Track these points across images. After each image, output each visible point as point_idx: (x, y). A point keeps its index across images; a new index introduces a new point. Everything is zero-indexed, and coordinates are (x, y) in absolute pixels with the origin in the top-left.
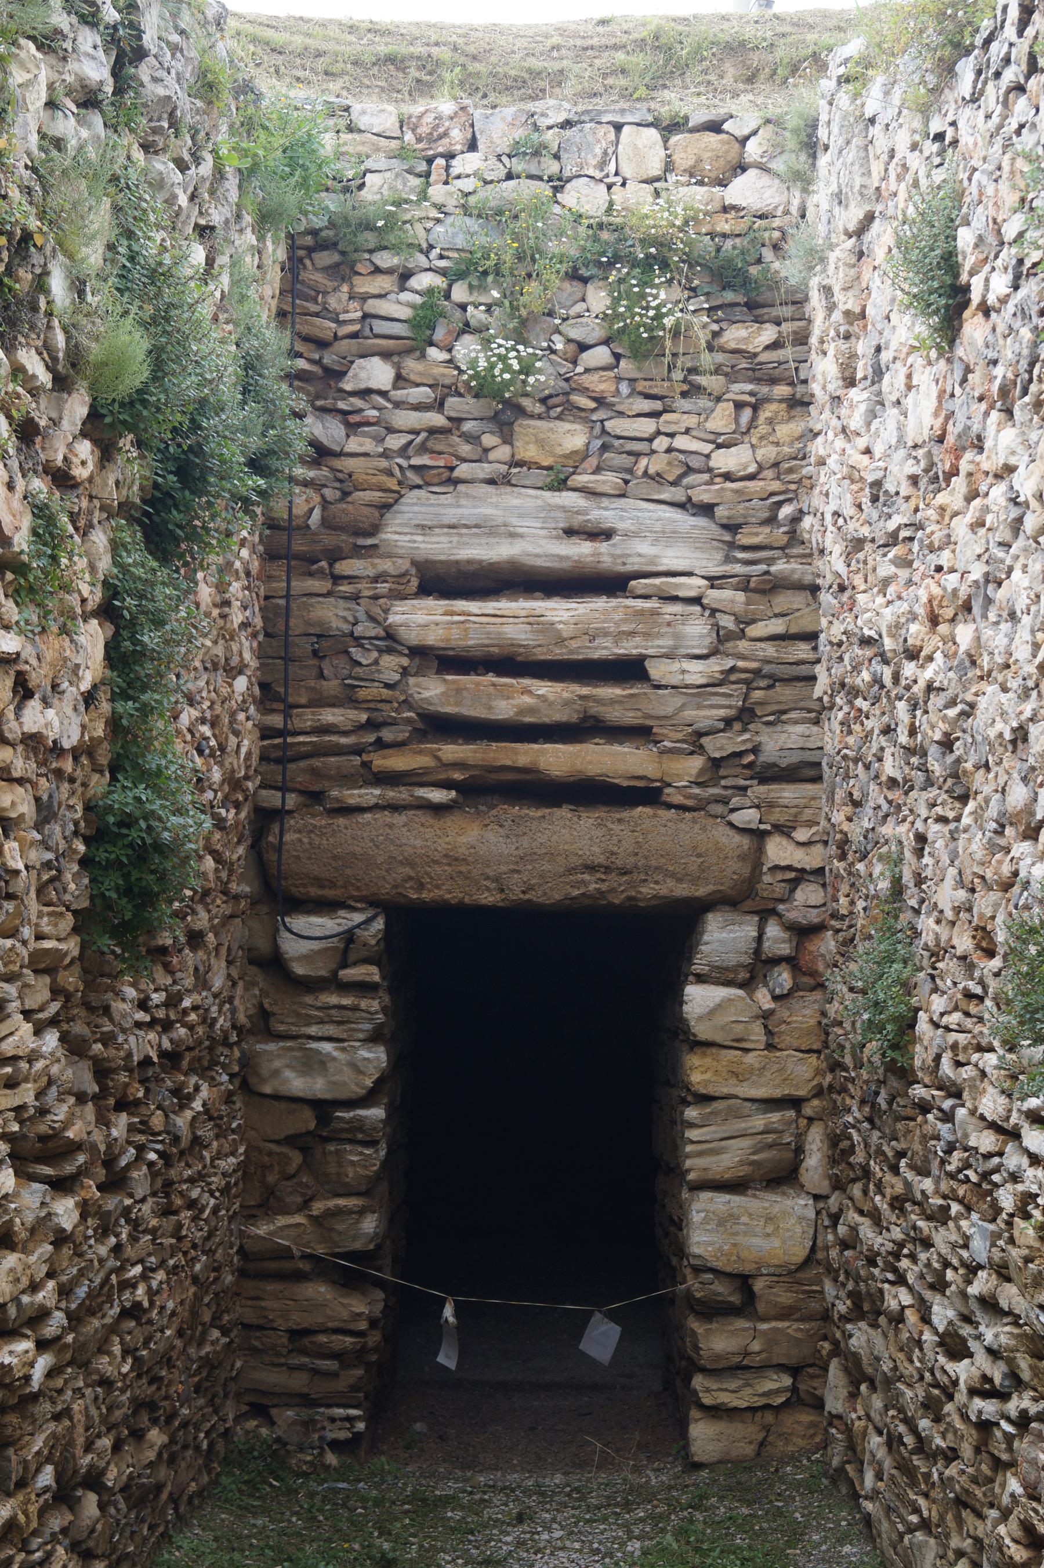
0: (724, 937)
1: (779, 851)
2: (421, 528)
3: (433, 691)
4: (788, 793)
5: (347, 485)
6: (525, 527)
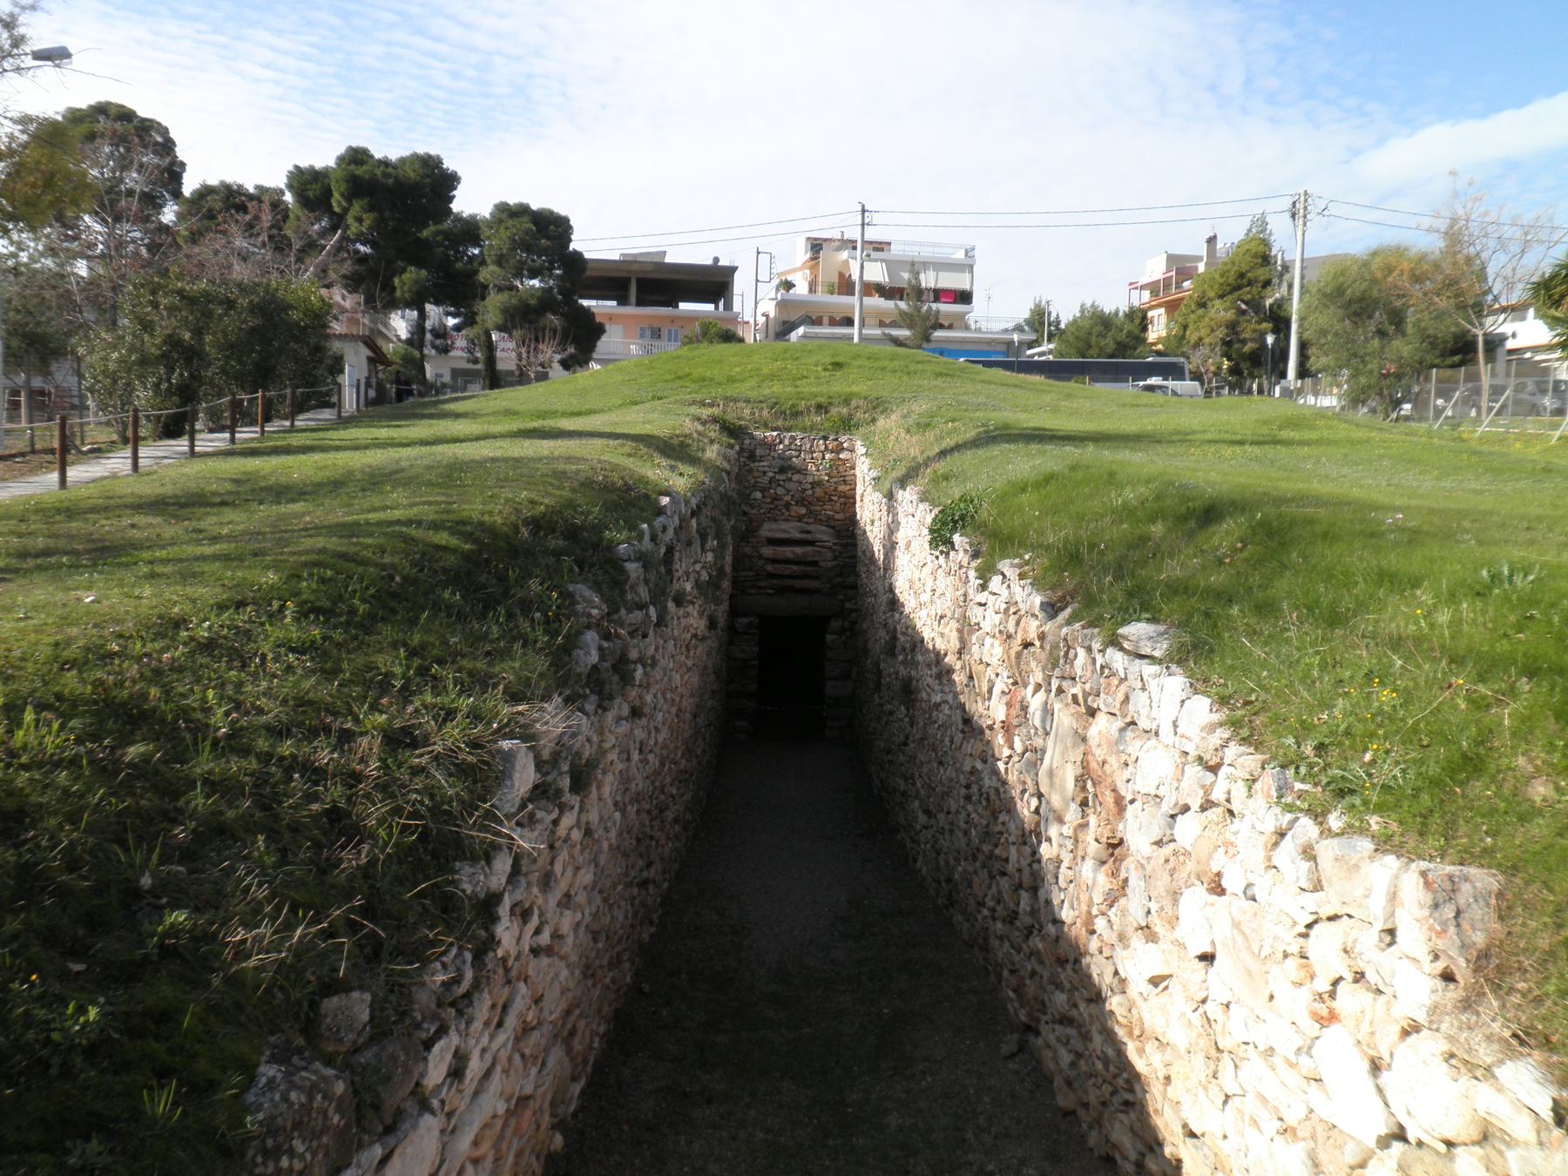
0: (835, 624)
1: (848, 605)
2: (768, 530)
3: (769, 568)
4: (850, 592)
5: (751, 520)
6: (791, 530)
